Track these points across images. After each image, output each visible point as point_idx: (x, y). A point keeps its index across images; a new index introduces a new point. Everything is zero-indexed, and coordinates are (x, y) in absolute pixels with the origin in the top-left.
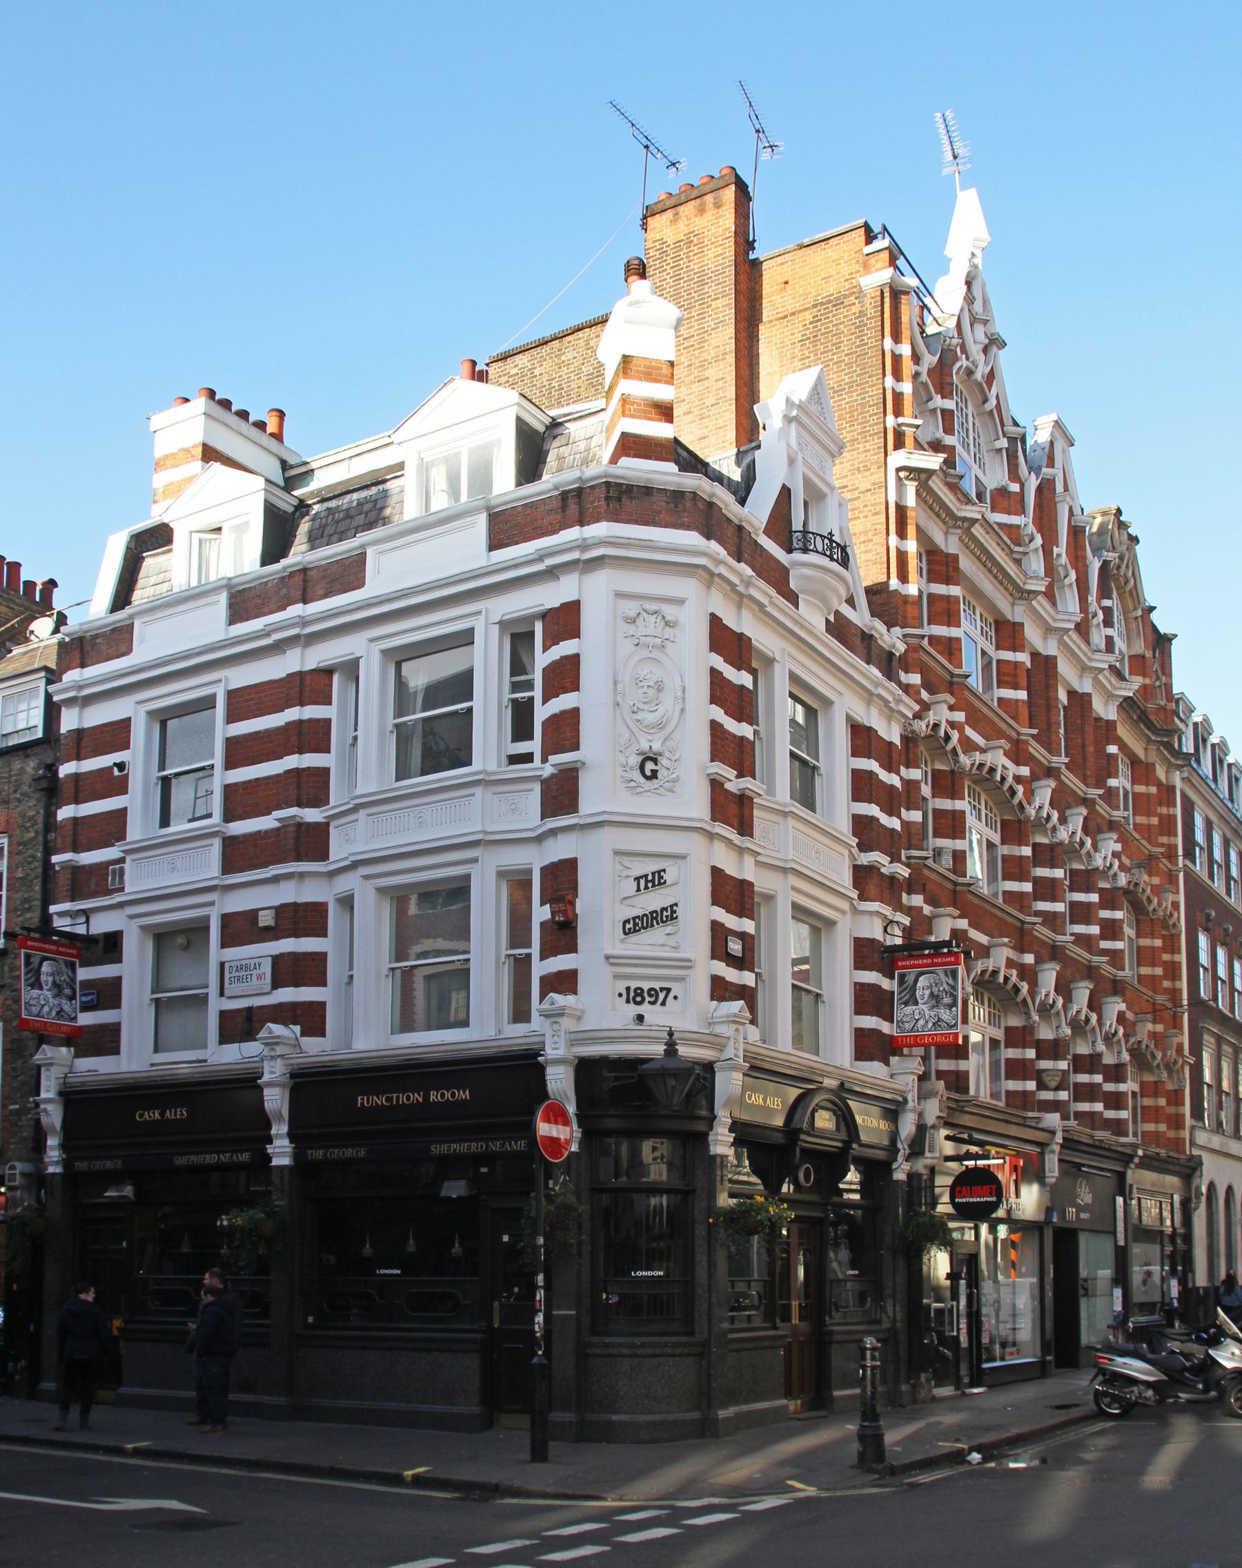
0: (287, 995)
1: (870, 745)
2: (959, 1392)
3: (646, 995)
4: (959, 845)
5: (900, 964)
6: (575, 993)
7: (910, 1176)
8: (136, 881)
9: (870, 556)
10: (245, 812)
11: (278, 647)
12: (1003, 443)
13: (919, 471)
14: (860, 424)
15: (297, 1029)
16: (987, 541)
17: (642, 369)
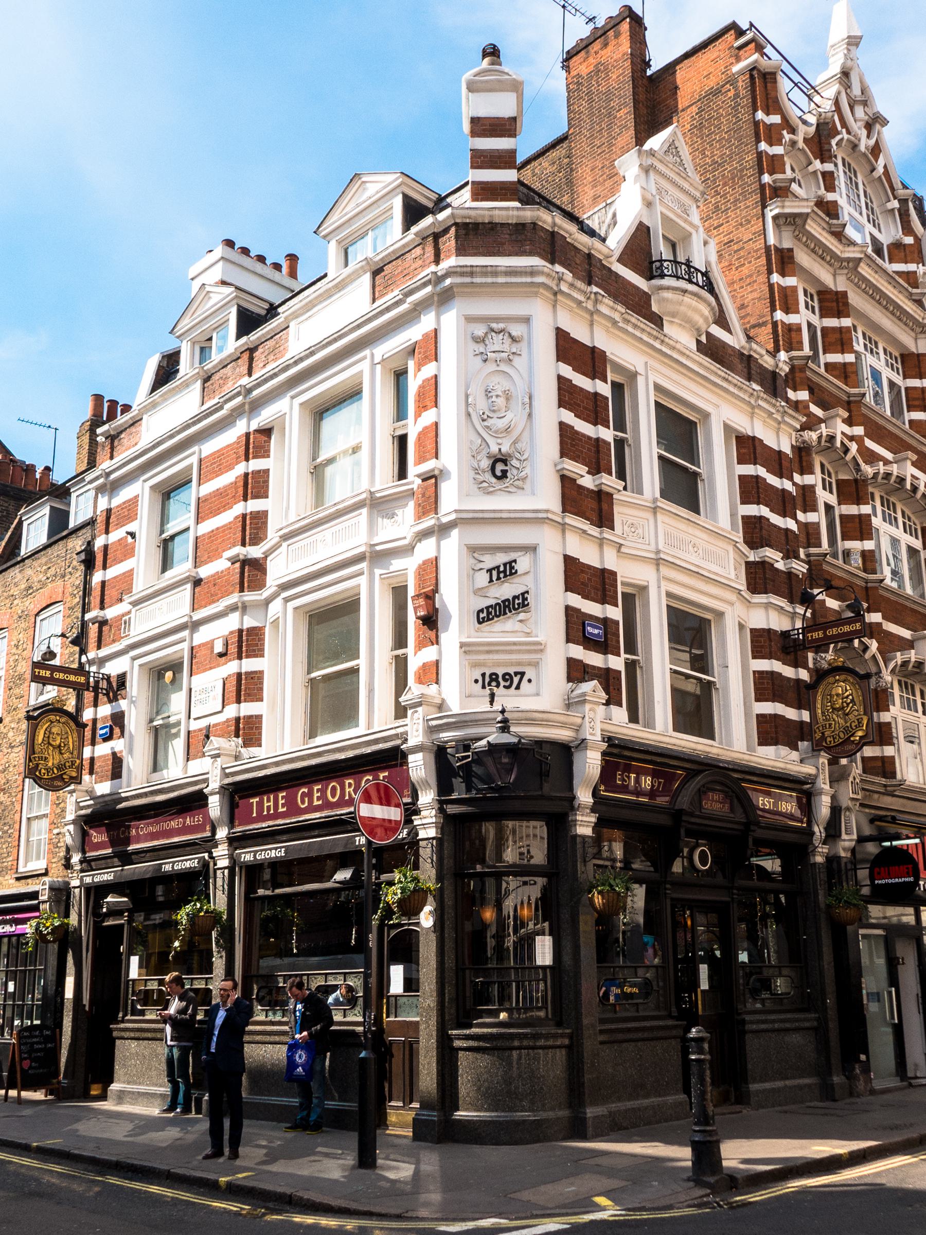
1: (755, 453)
2: (905, 1083)
3: (500, 679)
4: (869, 545)
12: (895, 204)
13: (795, 216)
16: (877, 280)
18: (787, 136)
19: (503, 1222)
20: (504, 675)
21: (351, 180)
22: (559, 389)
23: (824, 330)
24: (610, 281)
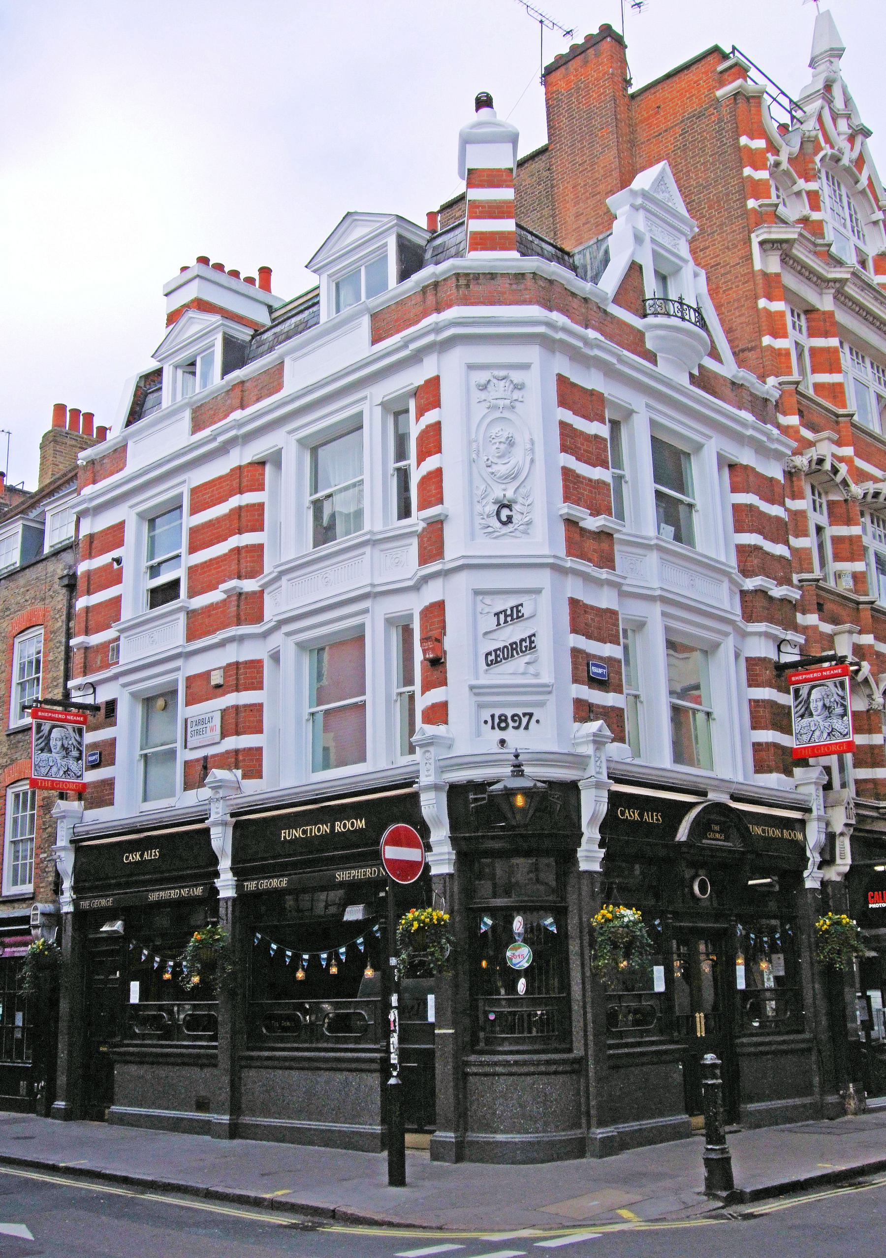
0: (232, 743)
3: (509, 720)
5: (793, 679)
6: (446, 723)
7: (823, 883)
8: (129, 655)
9: (743, 319)
10: (202, 588)
11: (224, 449)
14: (726, 210)
15: (239, 773)
16: (864, 298)
17: (485, 178)
18: (771, 158)
19: (538, 1233)
20: (513, 716)
21: (344, 218)
22: (561, 434)
23: (813, 350)
24: (605, 322)
